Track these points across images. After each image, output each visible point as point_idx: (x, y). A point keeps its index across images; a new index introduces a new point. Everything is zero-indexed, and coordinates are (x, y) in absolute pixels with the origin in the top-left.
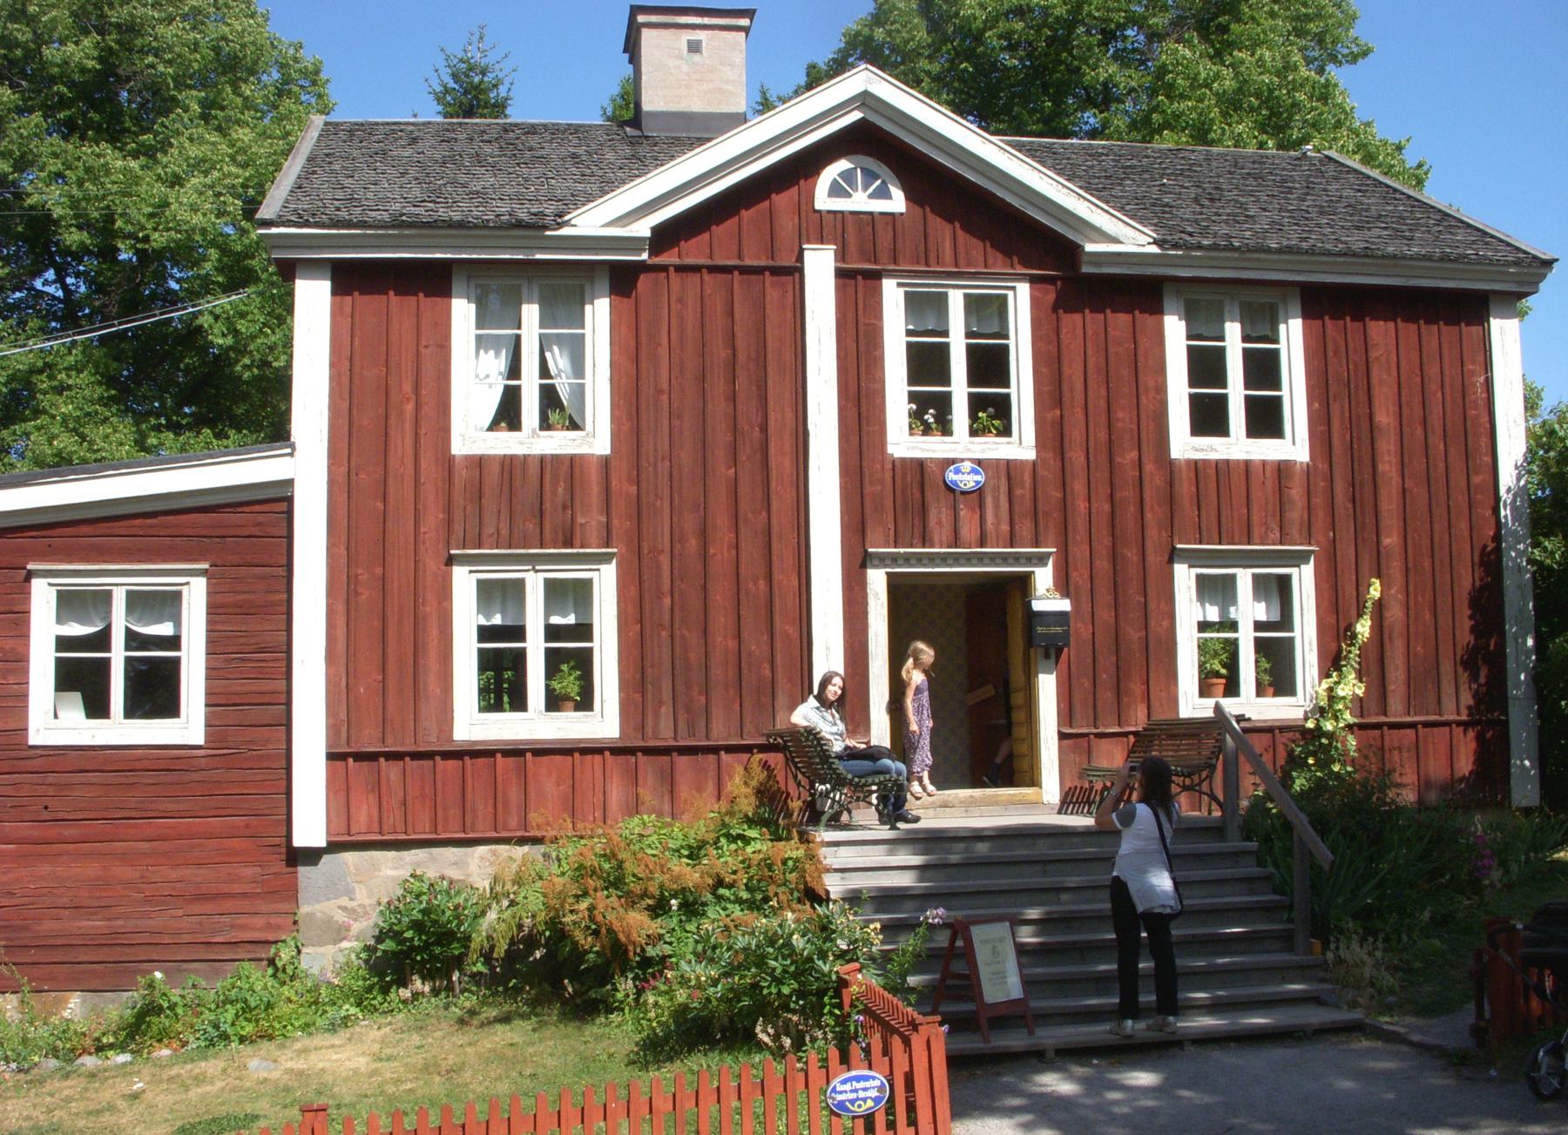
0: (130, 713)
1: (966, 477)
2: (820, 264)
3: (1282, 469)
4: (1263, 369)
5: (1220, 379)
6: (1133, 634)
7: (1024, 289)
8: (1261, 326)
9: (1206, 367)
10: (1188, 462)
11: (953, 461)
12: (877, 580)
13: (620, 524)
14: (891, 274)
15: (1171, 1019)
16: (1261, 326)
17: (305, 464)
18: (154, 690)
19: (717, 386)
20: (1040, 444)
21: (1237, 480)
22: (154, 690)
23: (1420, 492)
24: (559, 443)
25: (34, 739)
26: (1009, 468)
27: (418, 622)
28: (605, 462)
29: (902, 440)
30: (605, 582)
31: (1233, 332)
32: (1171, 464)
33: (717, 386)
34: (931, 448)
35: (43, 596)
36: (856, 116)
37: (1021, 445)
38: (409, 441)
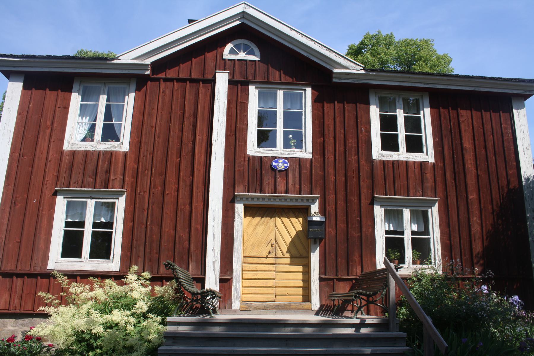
1: (281, 164)
2: (222, 80)
3: (422, 165)
6: (355, 234)
7: (309, 91)
8: (413, 107)
10: (380, 161)
11: (275, 158)
16: (413, 107)
20: (314, 153)
26: (300, 160)
28: (126, 154)
29: (253, 149)
34: (266, 152)
37: (306, 152)
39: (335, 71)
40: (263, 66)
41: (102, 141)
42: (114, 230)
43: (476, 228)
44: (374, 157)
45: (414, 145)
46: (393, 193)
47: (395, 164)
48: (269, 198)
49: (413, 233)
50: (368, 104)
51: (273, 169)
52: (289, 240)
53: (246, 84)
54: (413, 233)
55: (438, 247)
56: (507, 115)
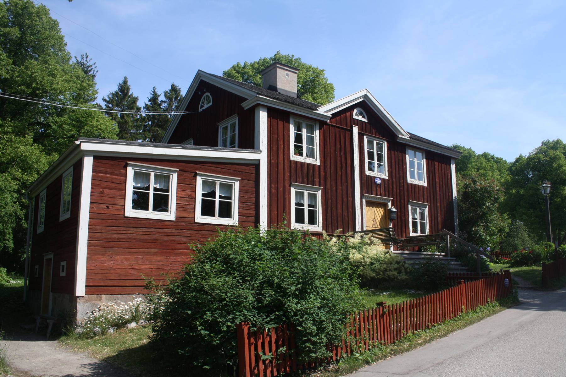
0: (154, 209)
4: (311, 141)
5: (414, 168)
6: (403, 218)
7: (386, 143)
8: (311, 130)
9: (298, 139)
12: (364, 201)
13: (322, 182)
14: (366, 135)
15: (171, 300)
16: (311, 130)
17: (262, 156)
18: (161, 203)
19: (338, 153)
20: (389, 176)
21: (311, 168)
22: (226, 211)
23: (442, 195)
24: (309, 161)
25: (197, 221)
27: (284, 199)
30: (319, 194)
31: (304, 130)
32: (290, 161)
33: (338, 153)
35: (130, 172)
36: (362, 99)
38: (282, 155)
39: (400, 136)
40: (368, 126)
41: (314, 158)
42: (170, 194)
43: (439, 219)
44: (408, 182)
45: (311, 154)
46: (387, 195)
47: (302, 164)
48: (373, 197)
49: (155, 189)
50: (289, 124)
51: (375, 183)
52: (379, 219)
53: (363, 135)
54: (155, 189)
55: (428, 226)
56: (448, 166)
